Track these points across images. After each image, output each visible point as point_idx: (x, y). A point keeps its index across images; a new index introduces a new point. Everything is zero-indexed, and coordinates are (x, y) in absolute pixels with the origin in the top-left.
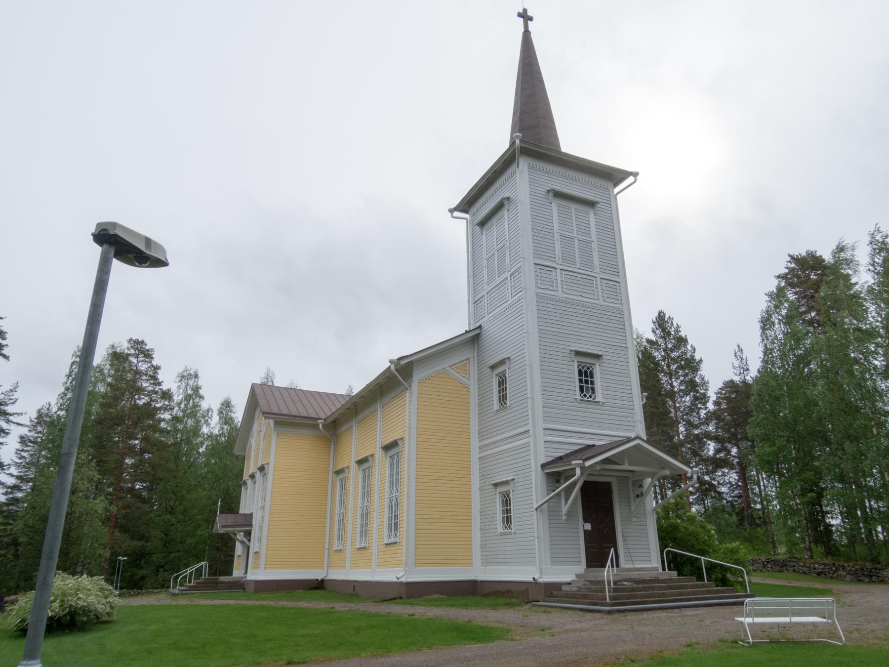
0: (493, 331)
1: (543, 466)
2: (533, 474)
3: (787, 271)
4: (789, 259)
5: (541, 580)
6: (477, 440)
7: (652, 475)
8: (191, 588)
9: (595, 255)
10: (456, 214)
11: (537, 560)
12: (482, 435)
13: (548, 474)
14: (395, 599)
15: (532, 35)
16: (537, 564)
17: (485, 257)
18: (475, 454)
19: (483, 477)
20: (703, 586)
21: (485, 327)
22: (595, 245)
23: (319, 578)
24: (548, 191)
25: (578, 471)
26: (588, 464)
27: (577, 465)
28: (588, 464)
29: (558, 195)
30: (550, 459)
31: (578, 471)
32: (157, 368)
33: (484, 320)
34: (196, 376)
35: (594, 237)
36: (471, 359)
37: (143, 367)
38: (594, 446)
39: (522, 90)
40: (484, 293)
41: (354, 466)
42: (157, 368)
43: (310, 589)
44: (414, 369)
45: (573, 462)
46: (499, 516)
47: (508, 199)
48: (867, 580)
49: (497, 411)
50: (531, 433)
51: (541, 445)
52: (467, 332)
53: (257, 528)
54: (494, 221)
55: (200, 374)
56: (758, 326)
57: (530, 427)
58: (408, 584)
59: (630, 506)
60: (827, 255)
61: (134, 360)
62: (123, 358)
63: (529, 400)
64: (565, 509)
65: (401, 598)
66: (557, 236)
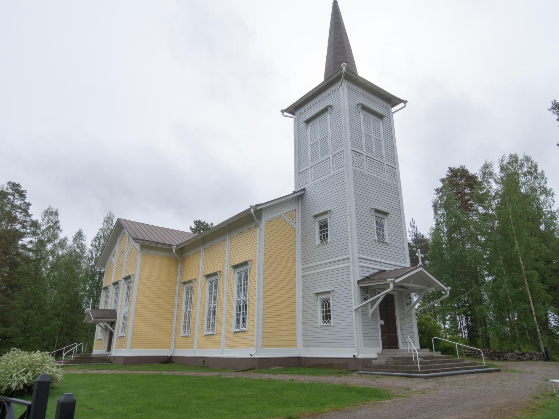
0: (313, 194)
1: (359, 282)
2: (353, 287)
3: (446, 177)
4: (448, 170)
5: (360, 356)
6: (301, 264)
7: (418, 292)
8: (72, 362)
9: (383, 149)
10: (285, 114)
11: (356, 343)
12: (304, 260)
13: (361, 287)
14: (250, 369)
15: (339, 4)
16: (356, 346)
17: (309, 143)
18: (299, 274)
19: (305, 289)
20: (456, 361)
21: (308, 190)
22: (383, 143)
23: (169, 355)
24: (358, 105)
25: (391, 286)
26: (397, 281)
27: (391, 281)
28: (397, 281)
29: (365, 108)
30: (362, 278)
31: (391, 286)
32: (29, 204)
33: (307, 185)
34: (56, 214)
35: (382, 138)
36: (297, 210)
37: (18, 203)
38: (385, 271)
39: (335, 38)
40: (309, 167)
41: (201, 279)
42: (29, 204)
43: (161, 363)
44: (263, 213)
45: (388, 280)
46: (320, 314)
47: (331, 106)
48: (497, 359)
49: (318, 245)
50: (351, 260)
51: (357, 268)
52: (294, 192)
53: (121, 321)
54: (318, 120)
55: (59, 213)
56: (432, 210)
57: (350, 256)
58: (259, 359)
59: (404, 310)
60: (474, 170)
61: (11, 198)
62: (3, 195)
63: (350, 238)
64: (371, 311)
65: (254, 369)
66: (363, 134)
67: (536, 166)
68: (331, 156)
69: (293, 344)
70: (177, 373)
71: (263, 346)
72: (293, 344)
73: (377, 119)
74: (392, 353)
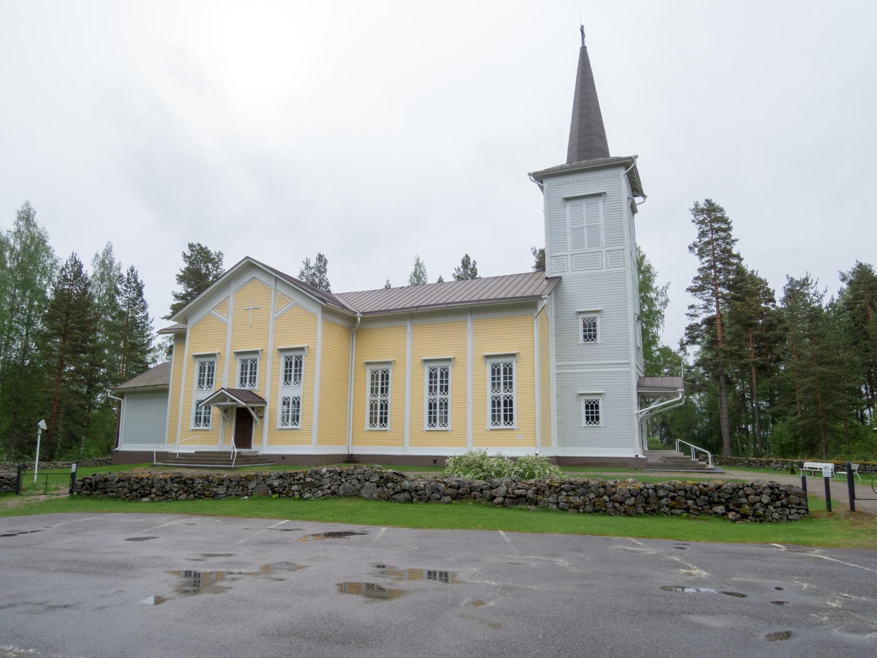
12: (559, 357)
15: (588, 50)
19: (561, 387)
21: (564, 280)
54: (584, 202)
68: (604, 250)
70: (600, 473)
74: (244, 451)
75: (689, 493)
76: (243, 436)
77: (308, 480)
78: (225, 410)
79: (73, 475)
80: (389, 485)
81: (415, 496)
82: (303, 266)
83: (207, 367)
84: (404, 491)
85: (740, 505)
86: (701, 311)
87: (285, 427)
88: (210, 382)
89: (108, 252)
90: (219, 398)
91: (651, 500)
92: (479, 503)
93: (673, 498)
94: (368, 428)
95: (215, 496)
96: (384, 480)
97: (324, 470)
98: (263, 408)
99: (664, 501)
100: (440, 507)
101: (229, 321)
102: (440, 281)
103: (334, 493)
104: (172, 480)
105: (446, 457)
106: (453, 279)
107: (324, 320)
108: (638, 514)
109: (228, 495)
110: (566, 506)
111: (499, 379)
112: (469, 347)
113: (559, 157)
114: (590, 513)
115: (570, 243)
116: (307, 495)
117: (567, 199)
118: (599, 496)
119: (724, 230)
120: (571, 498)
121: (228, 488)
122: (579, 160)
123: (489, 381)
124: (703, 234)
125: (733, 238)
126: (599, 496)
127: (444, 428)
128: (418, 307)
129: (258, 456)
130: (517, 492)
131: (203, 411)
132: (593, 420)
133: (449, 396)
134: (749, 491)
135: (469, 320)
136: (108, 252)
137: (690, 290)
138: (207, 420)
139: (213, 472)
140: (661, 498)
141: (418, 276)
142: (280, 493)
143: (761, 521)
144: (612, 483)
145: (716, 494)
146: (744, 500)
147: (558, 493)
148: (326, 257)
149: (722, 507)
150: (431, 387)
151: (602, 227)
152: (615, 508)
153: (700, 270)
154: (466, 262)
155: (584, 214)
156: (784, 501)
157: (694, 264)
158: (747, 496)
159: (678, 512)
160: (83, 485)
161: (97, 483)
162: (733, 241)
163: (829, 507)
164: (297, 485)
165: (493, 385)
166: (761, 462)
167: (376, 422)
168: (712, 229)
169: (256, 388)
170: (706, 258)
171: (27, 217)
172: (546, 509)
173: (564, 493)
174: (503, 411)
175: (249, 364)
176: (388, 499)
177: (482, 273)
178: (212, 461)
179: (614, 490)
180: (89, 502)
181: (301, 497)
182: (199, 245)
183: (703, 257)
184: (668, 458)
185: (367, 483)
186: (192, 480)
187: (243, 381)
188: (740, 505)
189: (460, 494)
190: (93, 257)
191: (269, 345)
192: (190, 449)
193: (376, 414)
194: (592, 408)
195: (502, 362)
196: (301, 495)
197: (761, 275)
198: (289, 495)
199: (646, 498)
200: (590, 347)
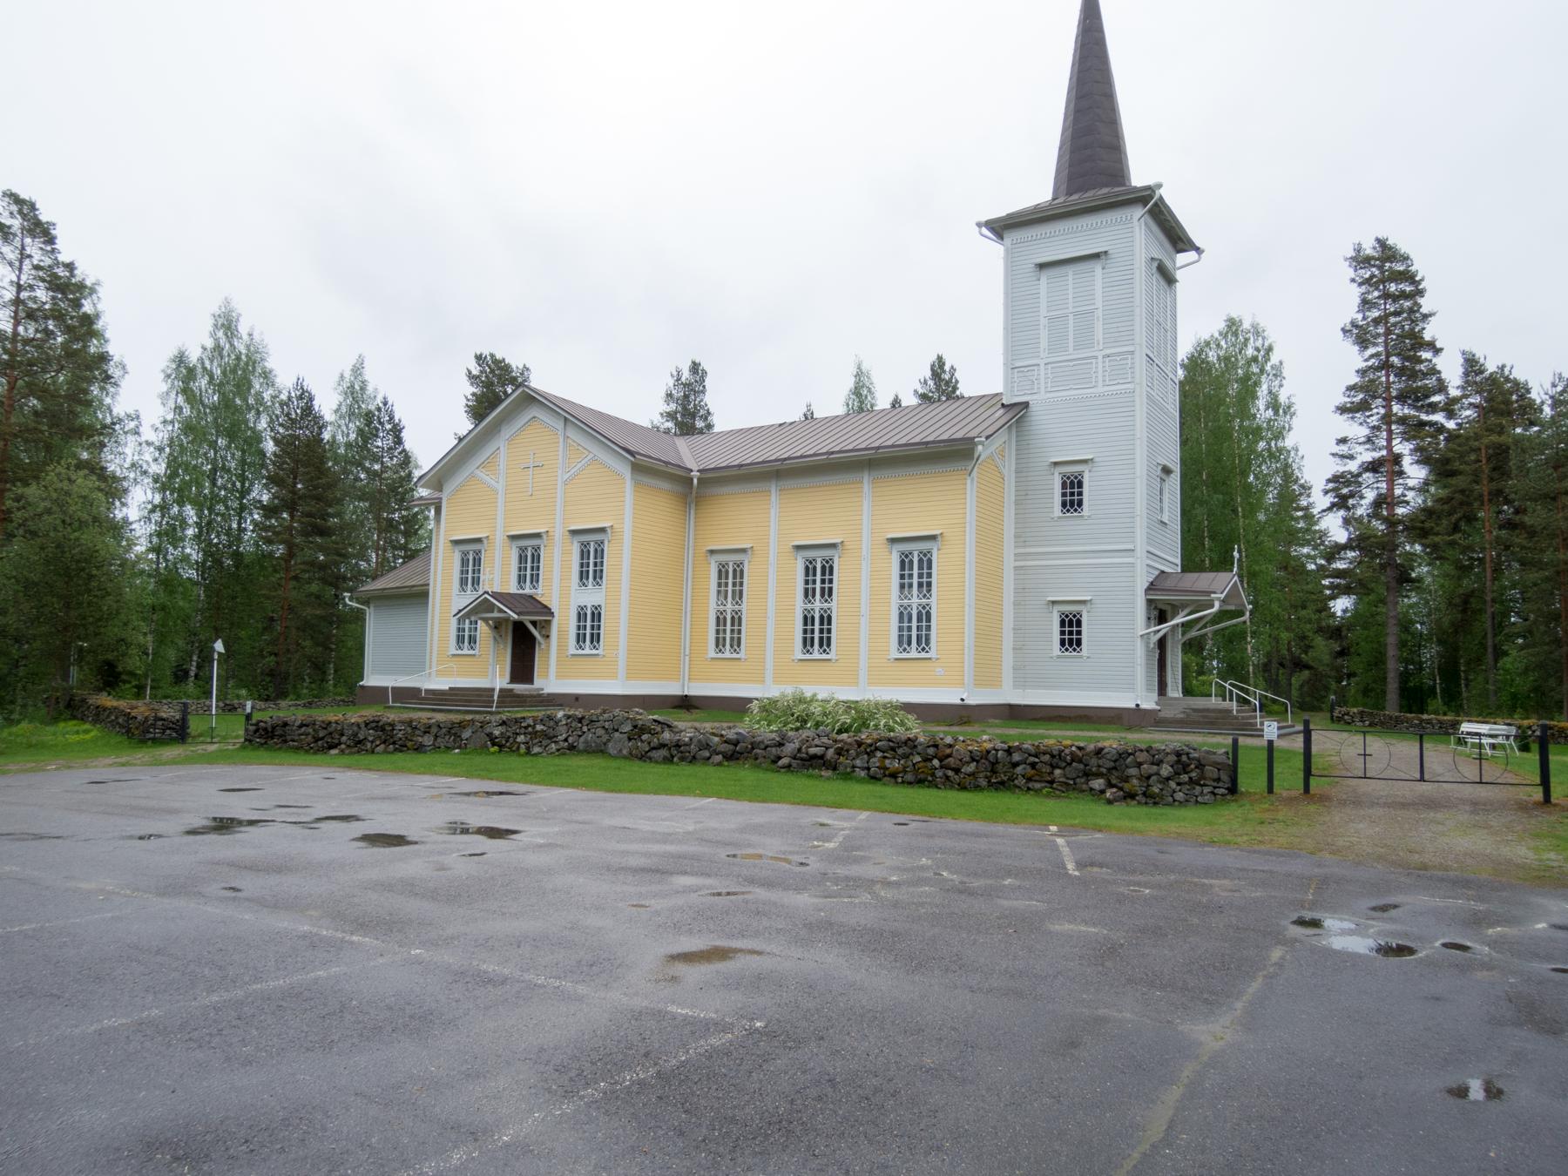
10: (984, 230)
17: (1043, 312)
19: (1020, 591)
21: (1033, 407)
54: (1070, 270)
67: (1270, 349)
69: (994, 682)
70: (1029, 731)
71: (628, 678)
72: (419, 666)
73: (1162, 282)
74: (519, 688)
75: (1057, 758)
76: (523, 668)
77: (539, 727)
78: (497, 626)
79: (248, 717)
80: (645, 737)
81: (679, 753)
82: (671, 382)
83: (471, 554)
84: (663, 746)
85: (1126, 779)
86: (1360, 449)
87: (905, 655)
88: (476, 581)
89: (357, 370)
90: (482, 608)
91: (999, 767)
92: (758, 766)
93: (1033, 765)
94: (712, 654)
95: (419, 749)
96: (639, 730)
97: (560, 714)
98: (549, 622)
99: (1019, 769)
100: (709, 770)
101: (500, 487)
102: (896, 403)
103: (572, 748)
104: (367, 725)
105: (750, 700)
106: (914, 401)
107: (637, 484)
108: (978, 788)
109: (436, 748)
110: (879, 773)
111: (911, 576)
112: (863, 522)
113: (1038, 188)
114: (910, 783)
115: (1044, 343)
116: (536, 750)
117: (1042, 266)
118: (927, 760)
119: (1404, 295)
120: (887, 762)
121: (436, 737)
122: (1069, 194)
123: (896, 581)
124: (1365, 304)
125: (1424, 310)
126: (927, 760)
127: (923, 655)
128: (878, 448)
129: (540, 695)
130: (813, 751)
131: (467, 626)
132: (1071, 644)
133: (834, 605)
134: (1142, 757)
135: (866, 480)
136: (357, 370)
137: (1342, 410)
138: (472, 640)
139: (415, 715)
140: (1015, 765)
141: (860, 393)
142: (501, 746)
143: (1155, 804)
144: (949, 740)
145: (1094, 761)
146: (1133, 771)
147: (870, 754)
148: (705, 365)
149: (1101, 781)
150: (806, 591)
151: (1099, 313)
152: (947, 778)
153: (1362, 372)
154: (938, 368)
155: (1070, 291)
156: (1193, 775)
157: (1350, 362)
158: (1139, 765)
159: (1037, 785)
160: (256, 731)
161: (274, 728)
162: (1426, 317)
163: (1270, 790)
164: (656, 740)
165: (902, 586)
166: (1440, 722)
167: (909, 644)
168: (1386, 296)
169: (540, 591)
170: (1371, 351)
171: (227, 324)
172: (848, 776)
173: (879, 754)
174: (818, 632)
175: (529, 552)
176: (643, 757)
177: (965, 389)
178: (468, 702)
179: (948, 751)
180: (262, 753)
181: (528, 752)
182: (492, 356)
183: (1366, 348)
184: (1195, 710)
185: (617, 735)
186: (392, 725)
187: (521, 580)
188: (1126, 779)
189: (737, 752)
190: (337, 378)
191: (555, 526)
192: (441, 684)
193: (910, 629)
194: (1071, 625)
195: (818, 555)
196: (528, 748)
197: (1519, 374)
198: (514, 750)
199: (993, 764)
200: (1072, 523)
